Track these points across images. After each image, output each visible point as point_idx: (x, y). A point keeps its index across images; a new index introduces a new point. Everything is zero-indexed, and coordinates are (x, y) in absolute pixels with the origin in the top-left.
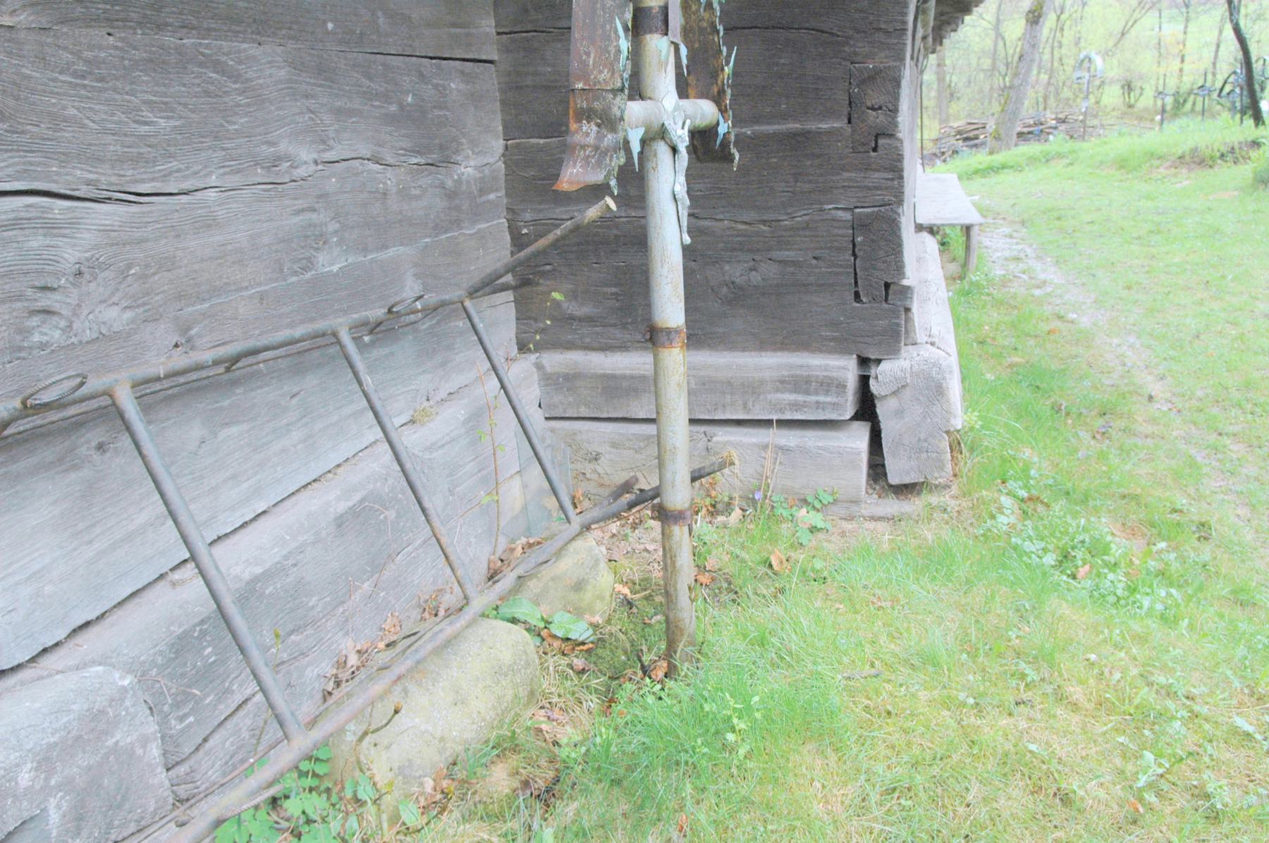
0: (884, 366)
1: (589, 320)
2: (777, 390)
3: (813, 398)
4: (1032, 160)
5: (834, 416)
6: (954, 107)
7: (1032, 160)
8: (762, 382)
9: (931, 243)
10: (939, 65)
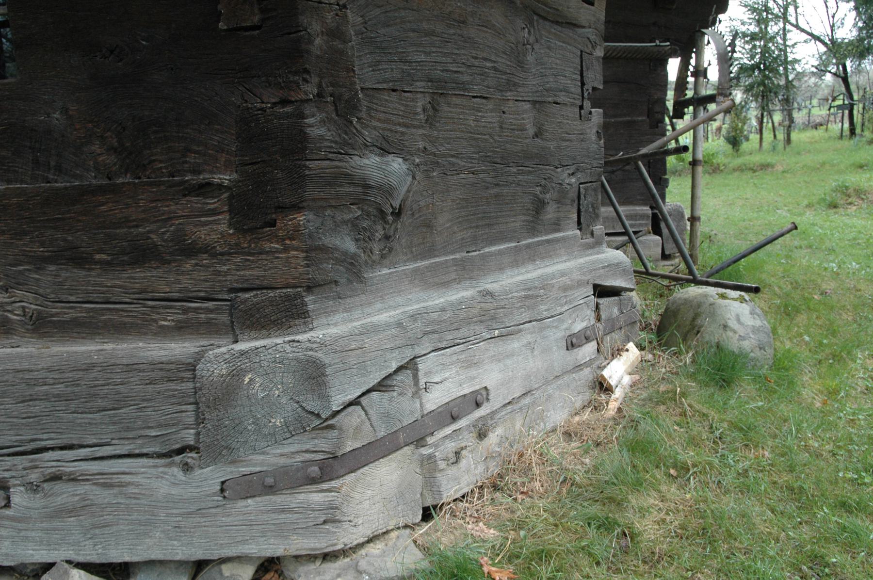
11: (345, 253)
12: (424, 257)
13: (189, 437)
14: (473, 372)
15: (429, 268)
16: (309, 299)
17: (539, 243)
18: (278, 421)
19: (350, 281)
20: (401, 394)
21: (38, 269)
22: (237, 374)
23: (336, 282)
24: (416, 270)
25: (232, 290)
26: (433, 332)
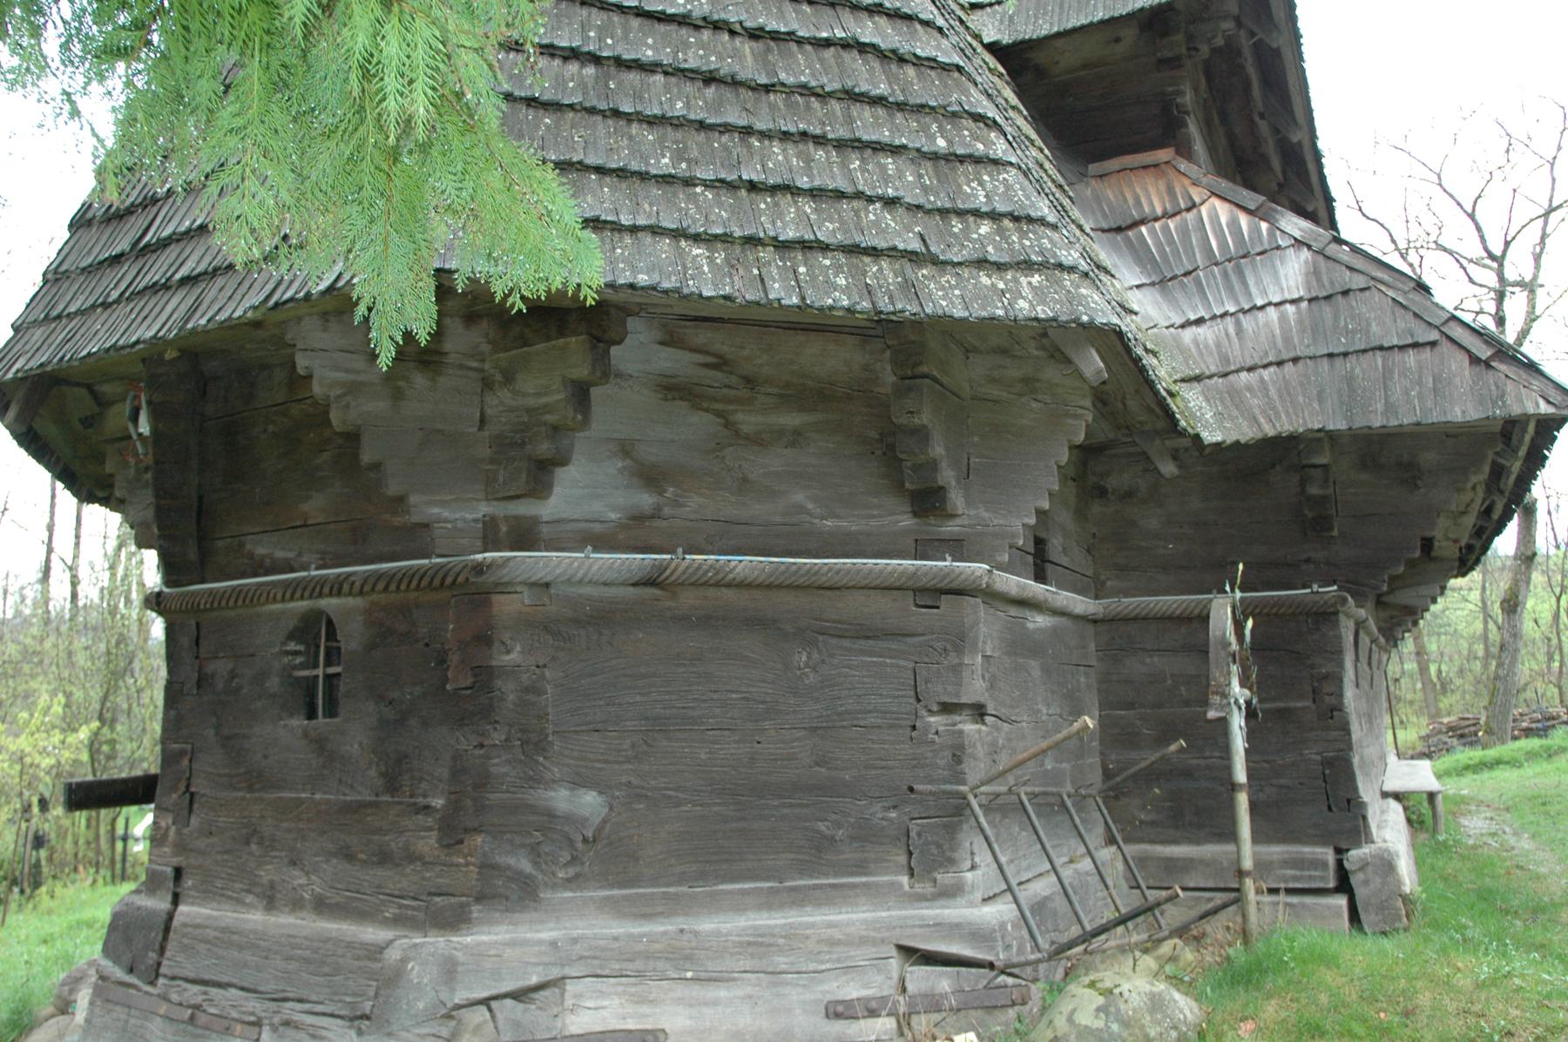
0: (1352, 853)
1: (1153, 823)
2: (1282, 868)
3: (1307, 873)
4: (1531, 756)
5: (1321, 885)
6: (1444, 703)
7: (1531, 756)
8: (1272, 862)
9: (1395, 808)
10: (1418, 654)
11: (520, 873)
12: (622, 885)
13: (367, 1006)
14: (646, 1009)
15: (625, 898)
16: (475, 908)
17: (815, 887)
18: (421, 1005)
19: (521, 899)
20: (540, 1008)
21: (327, 861)
22: (404, 961)
23: (507, 898)
24: (607, 898)
25: (430, 894)
26: (595, 958)
